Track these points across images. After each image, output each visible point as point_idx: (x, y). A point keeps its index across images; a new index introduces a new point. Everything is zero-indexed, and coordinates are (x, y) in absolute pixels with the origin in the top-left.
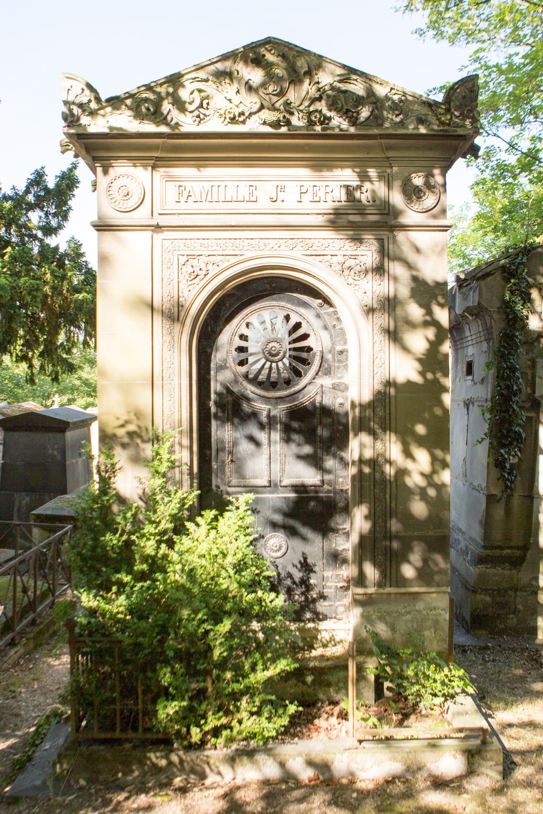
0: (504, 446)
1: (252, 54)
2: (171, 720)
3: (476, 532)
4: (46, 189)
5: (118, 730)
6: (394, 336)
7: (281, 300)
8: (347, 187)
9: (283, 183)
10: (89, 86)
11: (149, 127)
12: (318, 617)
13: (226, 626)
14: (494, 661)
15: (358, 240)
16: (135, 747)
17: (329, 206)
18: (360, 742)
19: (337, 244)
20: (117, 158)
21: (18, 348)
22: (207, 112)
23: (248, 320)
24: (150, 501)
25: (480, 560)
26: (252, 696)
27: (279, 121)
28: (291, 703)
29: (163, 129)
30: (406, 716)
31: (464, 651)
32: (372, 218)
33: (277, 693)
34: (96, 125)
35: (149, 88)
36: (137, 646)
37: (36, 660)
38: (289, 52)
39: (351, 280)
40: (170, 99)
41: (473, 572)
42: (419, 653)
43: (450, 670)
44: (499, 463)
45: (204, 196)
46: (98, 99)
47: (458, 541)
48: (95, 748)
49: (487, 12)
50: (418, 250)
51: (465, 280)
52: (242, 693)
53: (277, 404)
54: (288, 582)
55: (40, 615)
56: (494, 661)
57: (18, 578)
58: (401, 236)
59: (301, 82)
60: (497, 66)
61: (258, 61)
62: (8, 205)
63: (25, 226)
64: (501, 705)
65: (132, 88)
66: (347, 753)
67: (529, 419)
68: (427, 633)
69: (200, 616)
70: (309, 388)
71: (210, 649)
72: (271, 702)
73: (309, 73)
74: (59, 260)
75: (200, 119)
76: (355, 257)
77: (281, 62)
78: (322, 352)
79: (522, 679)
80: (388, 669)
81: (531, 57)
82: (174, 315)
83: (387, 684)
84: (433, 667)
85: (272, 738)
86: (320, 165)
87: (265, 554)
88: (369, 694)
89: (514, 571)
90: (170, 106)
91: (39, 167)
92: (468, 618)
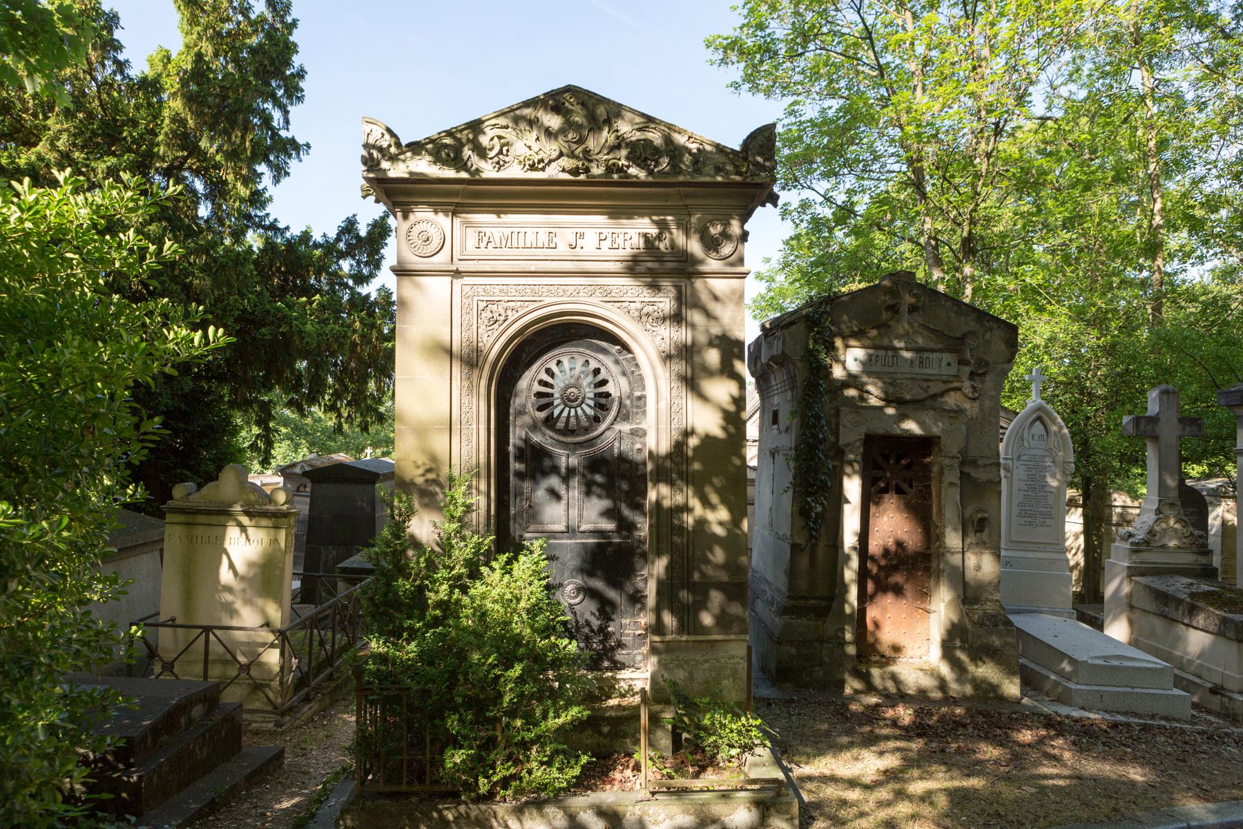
0: (810, 494)
1: (555, 101)
2: (458, 771)
3: (782, 583)
4: (358, 237)
5: (405, 780)
6: (691, 383)
7: (581, 346)
8: (645, 235)
9: (582, 230)
10: (389, 130)
11: (450, 173)
12: (618, 666)
13: (517, 670)
14: (799, 714)
15: (655, 287)
16: (421, 801)
17: (628, 252)
18: (653, 794)
19: (633, 291)
20: (417, 204)
21: (327, 397)
22: (507, 159)
23: (548, 366)
24: (446, 546)
25: (785, 611)
26: (543, 745)
27: (577, 168)
28: (584, 753)
29: (464, 175)
30: (703, 769)
31: (769, 704)
32: (670, 265)
33: (568, 742)
34: (396, 171)
35: (449, 133)
36: (425, 693)
37: (331, 716)
38: (588, 100)
39: (649, 327)
40: (470, 146)
41: (777, 622)
42: (716, 703)
43: (747, 719)
44: (803, 512)
45: (504, 242)
46: (398, 144)
47: (764, 591)
48: (381, 802)
49: (802, 64)
50: (716, 298)
51: (771, 329)
52: (533, 742)
53: (575, 450)
54: (586, 630)
55: (338, 669)
56: (799, 714)
57: (315, 631)
58: (699, 284)
59: (600, 129)
60: (811, 121)
61: (557, 109)
62: (318, 252)
63: (335, 274)
64: (803, 758)
65: (432, 133)
66: (639, 806)
67: (835, 467)
68: (725, 682)
69: (490, 660)
70: (608, 433)
71: (500, 696)
72: (564, 752)
73: (608, 122)
74: (369, 308)
75: (500, 166)
76: (653, 304)
77: (578, 110)
78: (620, 398)
79: (827, 733)
80: (686, 719)
81: (844, 110)
82: (472, 360)
83: (685, 735)
84: (729, 716)
85: (563, 789)
86: (616, 213)
87: (562, 601)
88: (665, 741)
89: (820, 623)
90: (470, 152)
91: (350, 215)
92: (773, 670)
